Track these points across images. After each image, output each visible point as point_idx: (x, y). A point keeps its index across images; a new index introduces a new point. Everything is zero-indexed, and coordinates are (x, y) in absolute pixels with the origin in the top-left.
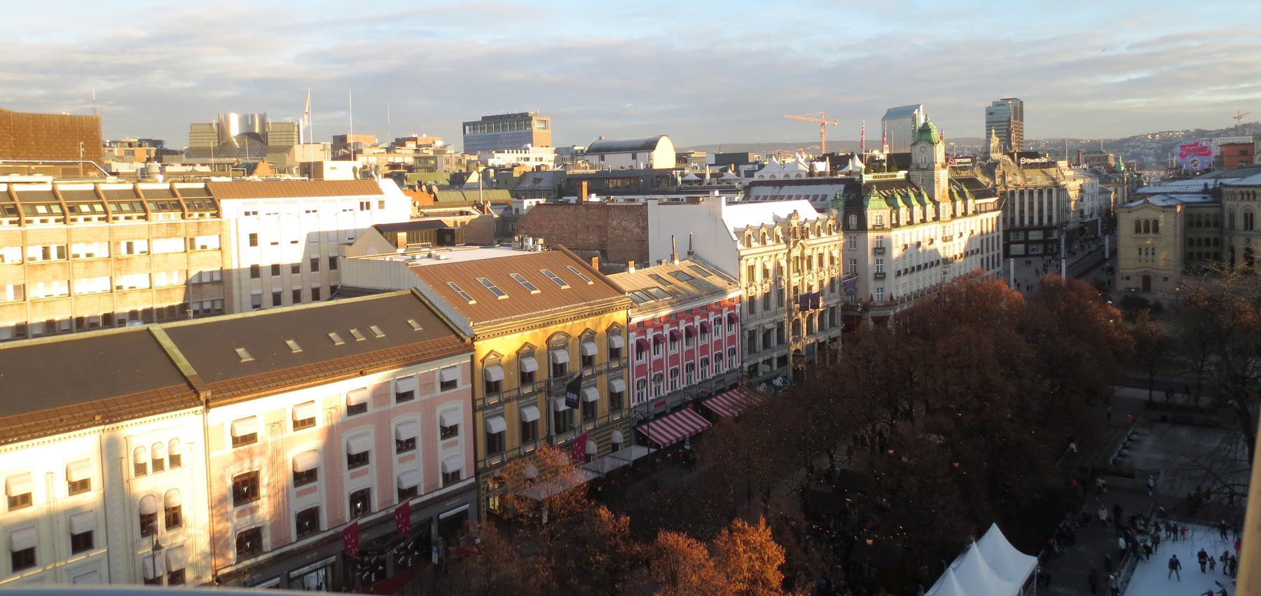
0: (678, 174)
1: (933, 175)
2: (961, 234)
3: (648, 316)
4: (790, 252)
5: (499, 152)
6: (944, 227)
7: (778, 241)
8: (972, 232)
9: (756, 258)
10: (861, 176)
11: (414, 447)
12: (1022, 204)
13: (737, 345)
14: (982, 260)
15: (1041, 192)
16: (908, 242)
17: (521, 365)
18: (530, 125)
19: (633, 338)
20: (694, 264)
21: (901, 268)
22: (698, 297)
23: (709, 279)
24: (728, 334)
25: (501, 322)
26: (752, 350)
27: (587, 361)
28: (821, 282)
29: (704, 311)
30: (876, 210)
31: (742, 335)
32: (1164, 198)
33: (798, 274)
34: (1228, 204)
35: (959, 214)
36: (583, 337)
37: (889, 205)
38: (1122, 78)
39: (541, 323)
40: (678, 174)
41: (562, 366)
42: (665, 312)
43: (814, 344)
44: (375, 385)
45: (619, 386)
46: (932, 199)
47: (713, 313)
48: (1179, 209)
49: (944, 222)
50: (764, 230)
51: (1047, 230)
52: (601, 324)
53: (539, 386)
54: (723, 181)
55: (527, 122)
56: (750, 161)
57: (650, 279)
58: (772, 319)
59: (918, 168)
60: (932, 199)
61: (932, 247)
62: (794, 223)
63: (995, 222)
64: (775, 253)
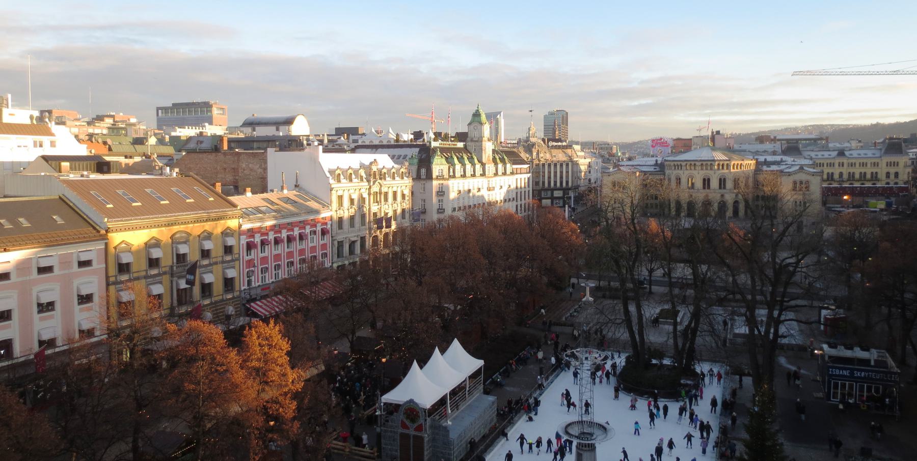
0: (304, 139)
1: (481, 145)
2: (501, 187)
3: (257, 225)
4: (370, 188)
5: (181, 128)
6: (489, 181)
7: (362, 180)
8: (510, 186)
9: (344, 190)
10: (430, 143)
11: (53, 310)
12: (549, 172)
13: (329, 251)
14: (517, 206)
15: (561, 165)
16: (461, 189)
17: (148, 253)
18: (211, 111)
19: (244, 240)
20: (298, 193)
21: (456, 206)
22: (297, 214)
23: (308, 203)
24: (321, 242)
25: (131, 220)
26: (340, 254)
27: (205, 254)
28: (395, 211)
29: (303, 224)
30: (439, 166)
31: (333, 244)
32: (630, 167)
33: (377, 204)
34: (667, 172)
35: (500, 173)
36: (202, 236)
37: (448, 162)
38: (636, 103)
39: (166, 223)
40: (304, 139)
41: (184, 255)
42: (270, 223)
43: (389, 253)
44: (19, 260)
45: (231, 273)
46: (480, 161)
47: (309, 226)
48: (638, 174)
49: (489, 177)
50: (350, 171)
51: (566, 190)
52: (218, 228)
53: (164, 269)
54: (337, 145)
55: (209, 109)
56: (360, 133)
57: (262, 201)
58: (356, 234)
59: (472, 141)
60: (480, 161)
61: (479, 194)
62: (374, 168)
63: (526, 181)
64: (359, 188)
